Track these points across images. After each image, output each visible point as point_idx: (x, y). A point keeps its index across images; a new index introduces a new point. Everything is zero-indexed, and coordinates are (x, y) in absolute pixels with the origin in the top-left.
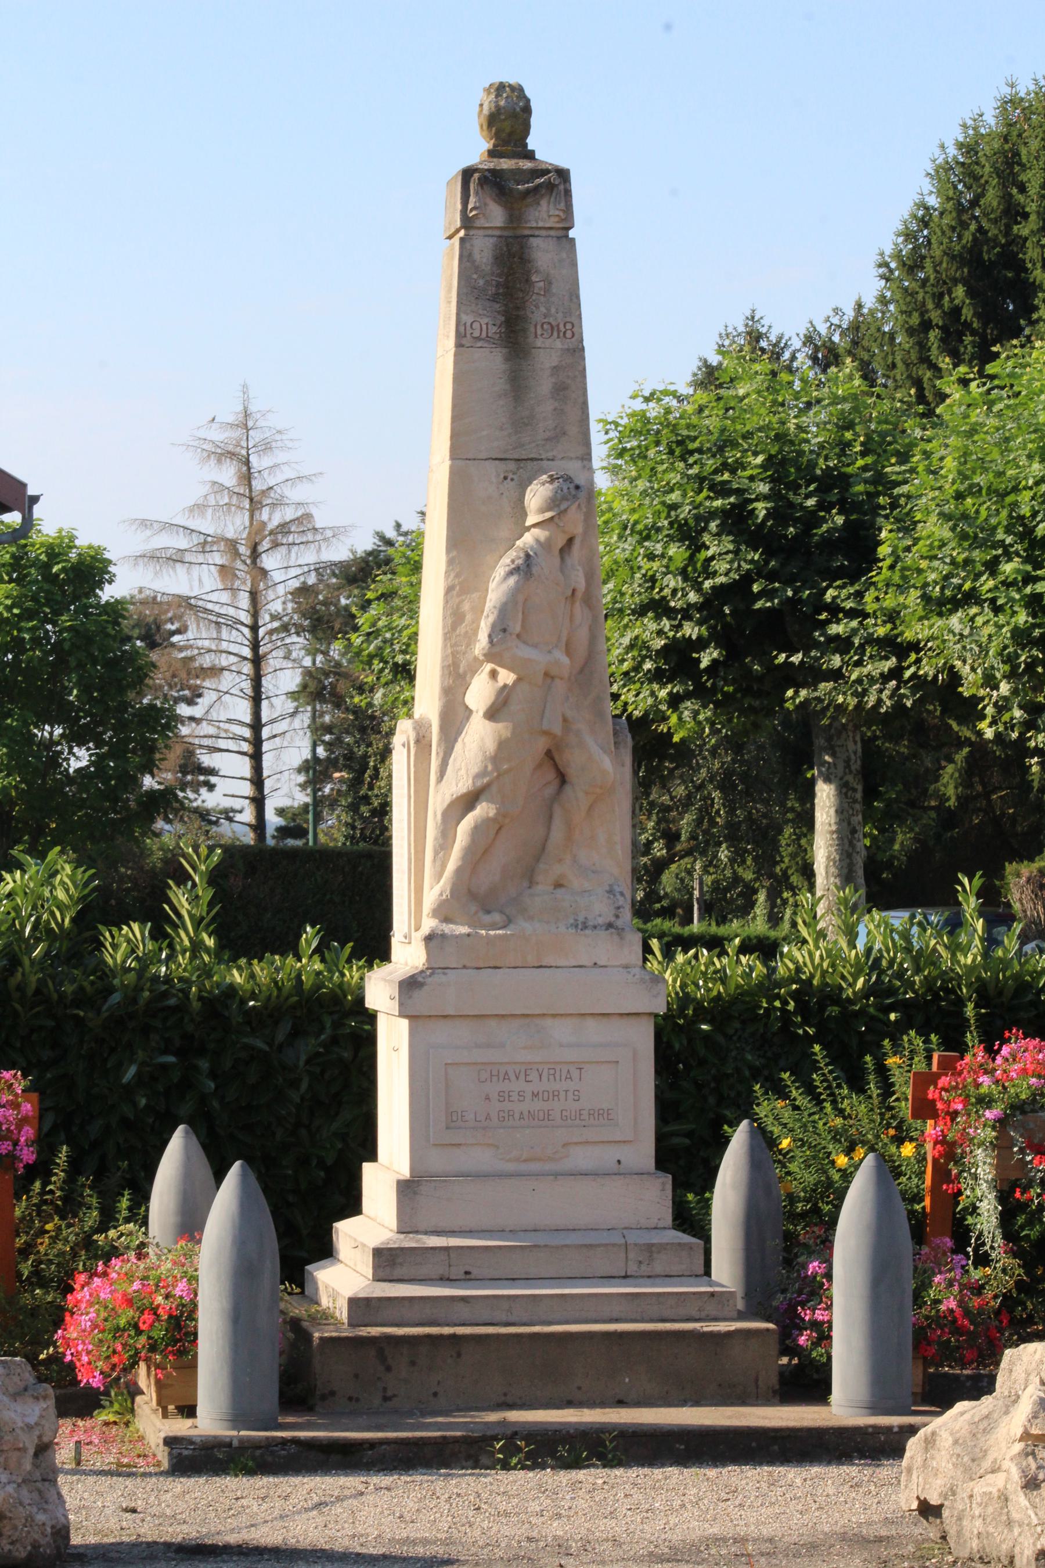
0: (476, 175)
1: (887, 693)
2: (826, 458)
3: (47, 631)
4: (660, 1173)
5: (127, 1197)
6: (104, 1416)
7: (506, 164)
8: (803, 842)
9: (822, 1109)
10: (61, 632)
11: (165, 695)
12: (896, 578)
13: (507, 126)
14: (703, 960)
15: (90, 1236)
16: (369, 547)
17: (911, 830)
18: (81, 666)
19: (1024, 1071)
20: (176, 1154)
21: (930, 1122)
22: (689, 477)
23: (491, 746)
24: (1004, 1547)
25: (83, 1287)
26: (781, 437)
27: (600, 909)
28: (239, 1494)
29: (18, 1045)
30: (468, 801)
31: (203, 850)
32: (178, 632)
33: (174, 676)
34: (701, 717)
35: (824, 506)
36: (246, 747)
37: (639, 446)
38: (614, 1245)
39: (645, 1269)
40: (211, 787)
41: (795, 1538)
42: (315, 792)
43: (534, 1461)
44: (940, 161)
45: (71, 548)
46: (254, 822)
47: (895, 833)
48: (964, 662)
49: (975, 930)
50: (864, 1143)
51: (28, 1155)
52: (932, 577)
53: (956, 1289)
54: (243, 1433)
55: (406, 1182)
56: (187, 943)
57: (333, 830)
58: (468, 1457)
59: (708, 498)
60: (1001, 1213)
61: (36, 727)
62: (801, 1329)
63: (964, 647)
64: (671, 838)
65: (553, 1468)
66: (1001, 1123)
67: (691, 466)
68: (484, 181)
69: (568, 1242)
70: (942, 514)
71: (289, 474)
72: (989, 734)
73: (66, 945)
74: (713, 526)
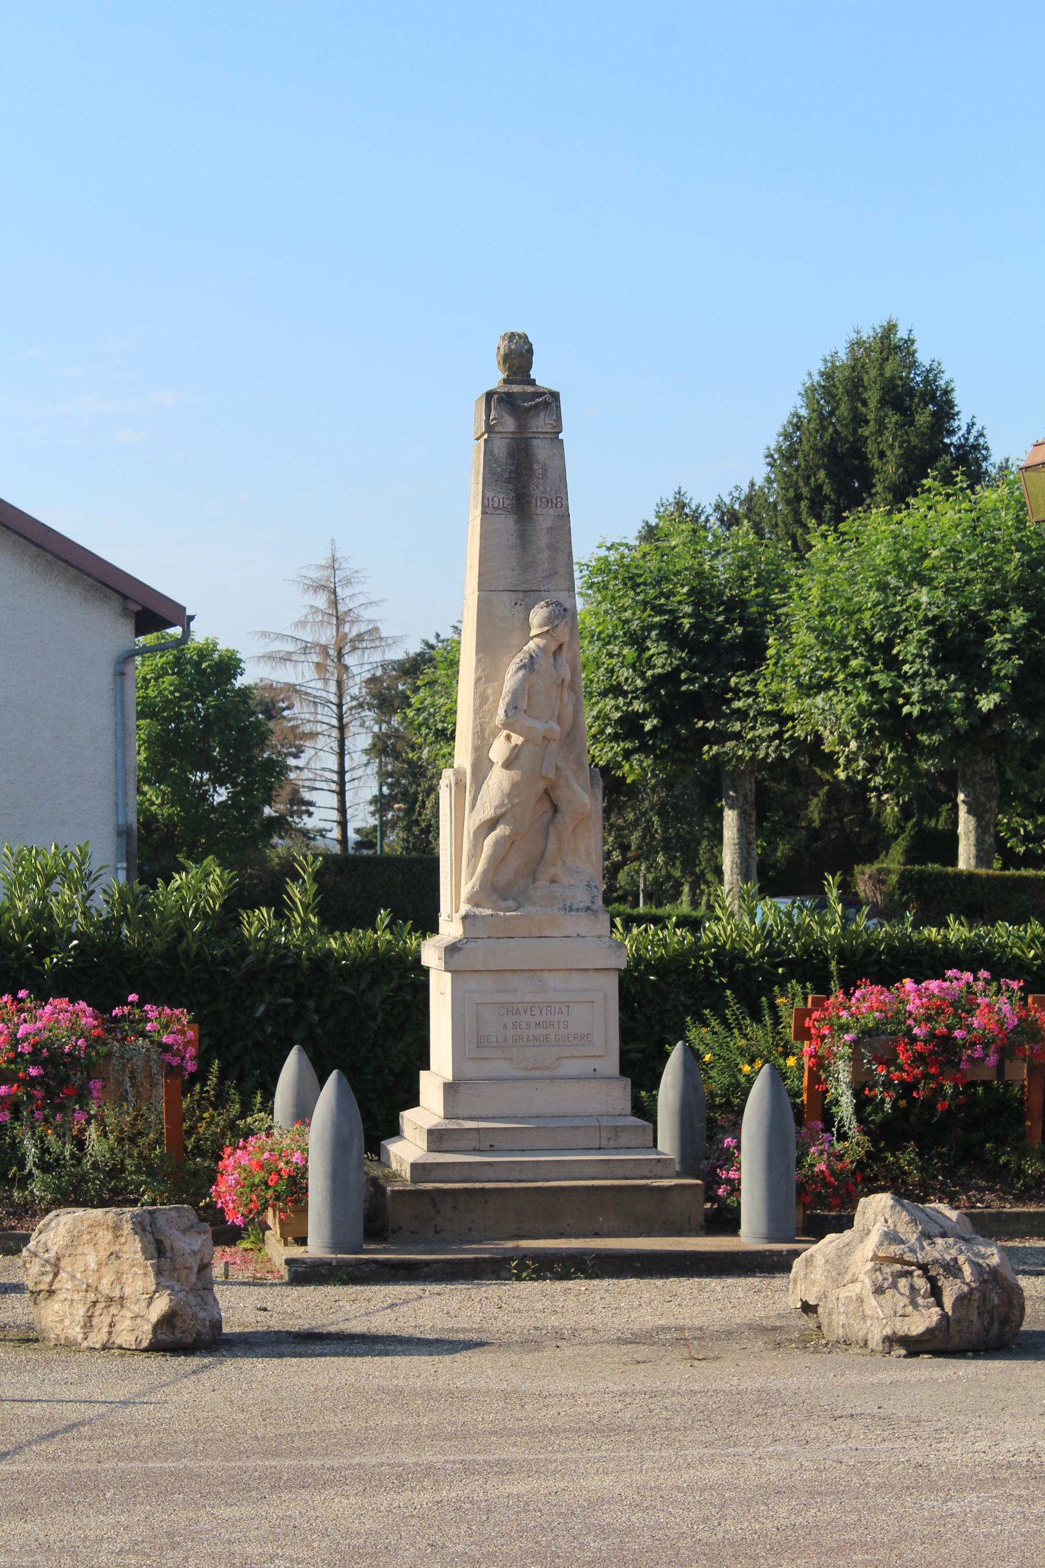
0: (496, 396)
1: (772, 748)
2: (731, 589)
3: (198, 708)
4: (623, 1078)
5: (259, 1095)
6: (245, 1244)
7: (516, 388)
8: (715, 851)
9: (733, 1033)
10: (208, 708)
11: (279, 752)
12: (779, 671)
13: (516, 362)
14: (650, 932)
15: (234, 1122)
16: (418, 651)
17: (789, 843)
18: (221, 731)
19: (871, 1007)
20: (292, 1066)
21: (806, 1043)
22: (637, 602)
23: (507, 787)
24: (861, 1333)
25: (229, 1156)
26: (699, 575)
27: (581, 897)
28: (337, 1298)
29: (184, 991)
30: (491, 824)
31: (310, 858)
32: (288, 708)
33: (285, 738)
34: (645, 764)
35: (729, 621)
36: (334, 787)
37: (603, 581)
38: (591, 1127)
39: (612, 1144)
40: (310, 814)
41: (717, 1327)
42: (381, 817)
43: (538, 1275)
44: (808, 384)
45: (214, 651)
46: (340, 838)
47: (777, 844)
48: (825, 728)
49: (836, 911)
50: (761, 1057)
51: (191, 1066)
52: (803, 670)
53: (825, 1156)
54: (339, 1256)
55: (450, 1083)
56: (299, 921)
57: (394, 842)
58: (493, 1272)
59: (650, 616)
60: (856, 1105)
61: (191, 773)
62: (720, 1184)
63: (825, 718)
64: (624, 848)
65: (551, 1279)
66: (856, 1044)
67: (639, 594)
68: (500, 400)
69: (560, 1124)
70: (809, 628)
71: (363, 599)
72: (842, 776)
73: (216, 922)
74: (654, 633)
